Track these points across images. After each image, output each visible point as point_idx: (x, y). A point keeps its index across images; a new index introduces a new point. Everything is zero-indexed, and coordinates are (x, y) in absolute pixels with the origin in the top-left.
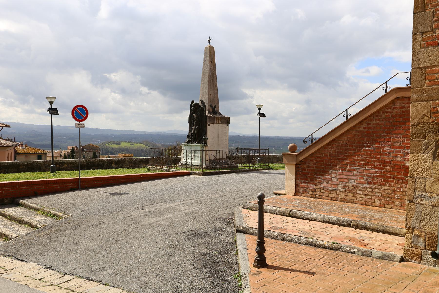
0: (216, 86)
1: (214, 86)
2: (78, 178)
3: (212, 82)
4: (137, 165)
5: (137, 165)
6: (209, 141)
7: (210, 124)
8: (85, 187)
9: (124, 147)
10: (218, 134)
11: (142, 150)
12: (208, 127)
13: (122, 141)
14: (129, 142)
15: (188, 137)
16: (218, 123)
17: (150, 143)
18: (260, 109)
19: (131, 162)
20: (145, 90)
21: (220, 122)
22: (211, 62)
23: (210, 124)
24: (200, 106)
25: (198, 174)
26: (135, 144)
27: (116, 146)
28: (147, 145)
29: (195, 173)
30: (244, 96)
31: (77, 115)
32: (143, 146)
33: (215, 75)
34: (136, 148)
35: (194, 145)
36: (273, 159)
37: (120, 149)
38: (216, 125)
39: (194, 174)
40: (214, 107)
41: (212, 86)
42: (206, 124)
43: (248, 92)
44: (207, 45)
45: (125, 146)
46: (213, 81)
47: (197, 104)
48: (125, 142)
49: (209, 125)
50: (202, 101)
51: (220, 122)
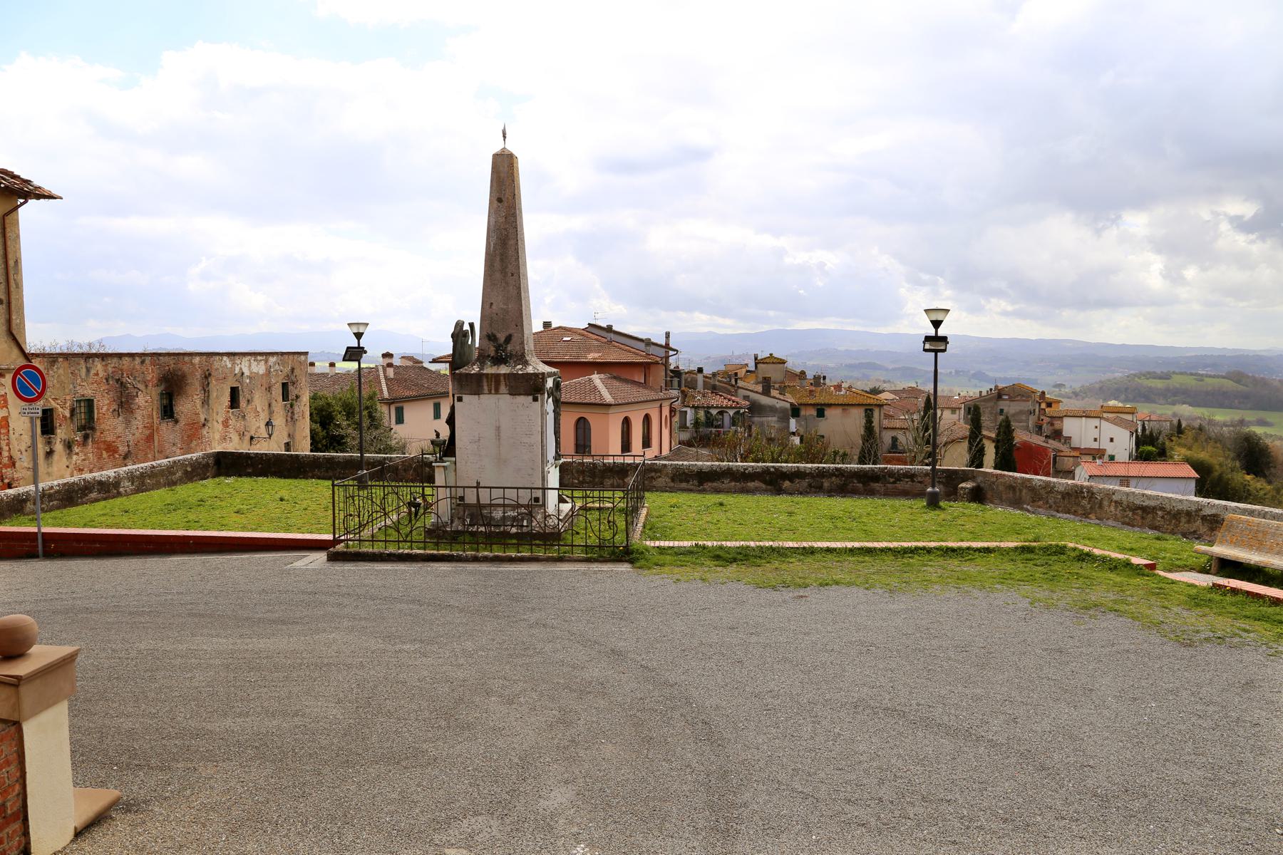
2: (35, 530)
7: (465, 398)
8: (49, 555)
10: (498, 429)
16: (497, 392)
18: (937, 324)
19: (583, 472)
21: (503, 388)
22: (500, 200)
23: (465, 398)
26: (1208, 380)
27: (1159, 384)
31: (23, 387)
33: (512, 242)
36: (1021, 491)
37: (1168, 390)
38: (487, 400)
41: (498, 275)
46: (502, 260)
51: (503, 388)
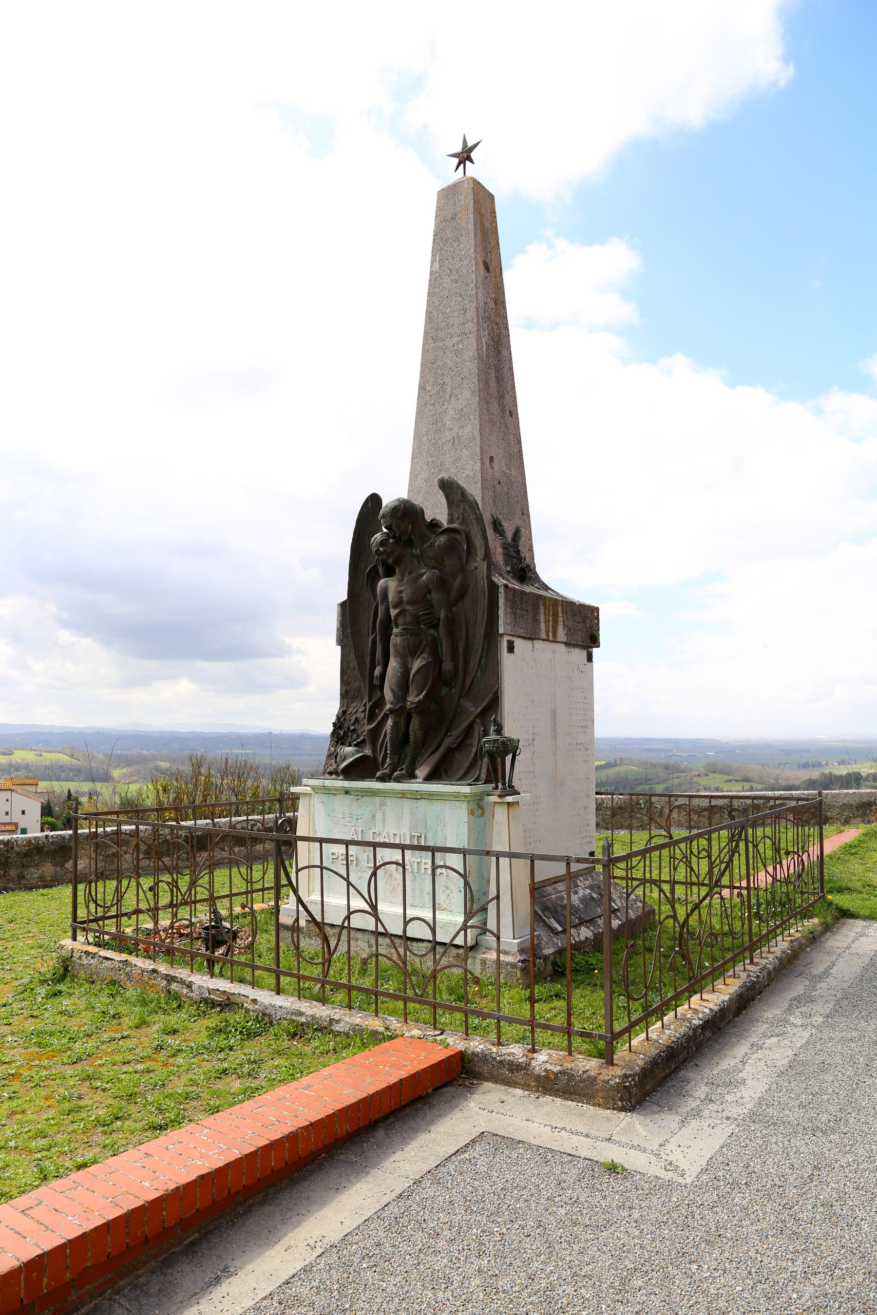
0: (513, 413)
1: (502, 406)
3: (493, 383)
4: (13, 873)
5: (13, 873)
6: (522, 770)
7: (519, 643)
9: (20, 761)
10: (554, 713)
11: (60, 766)
12: (507, 661)
13: (16, 749)
14: (31, 750)
15: (342, 732)
17: (79, 751)
20: (65, 636)
22: (487, 268)
23: (519, 643)
24: (434, 525)
25: (552, 1085)
26: (46, 755)
28: (72, 756)
29: (515, 1067)
30: (282, 651)
32: (64, 759)
34: (48, 763)
35: (403, 795)
37: (11, 765)
39: (512, 1074)
40: (509, 535)
41: (495, 407)
42: (491, 635)
43: (295, 642)
44: (451, 175)
45: (23, 759)
47: (406, 512)
48: (23, 749)
49: (511, 649)
50: (448, 487)
51: (562, 635)
